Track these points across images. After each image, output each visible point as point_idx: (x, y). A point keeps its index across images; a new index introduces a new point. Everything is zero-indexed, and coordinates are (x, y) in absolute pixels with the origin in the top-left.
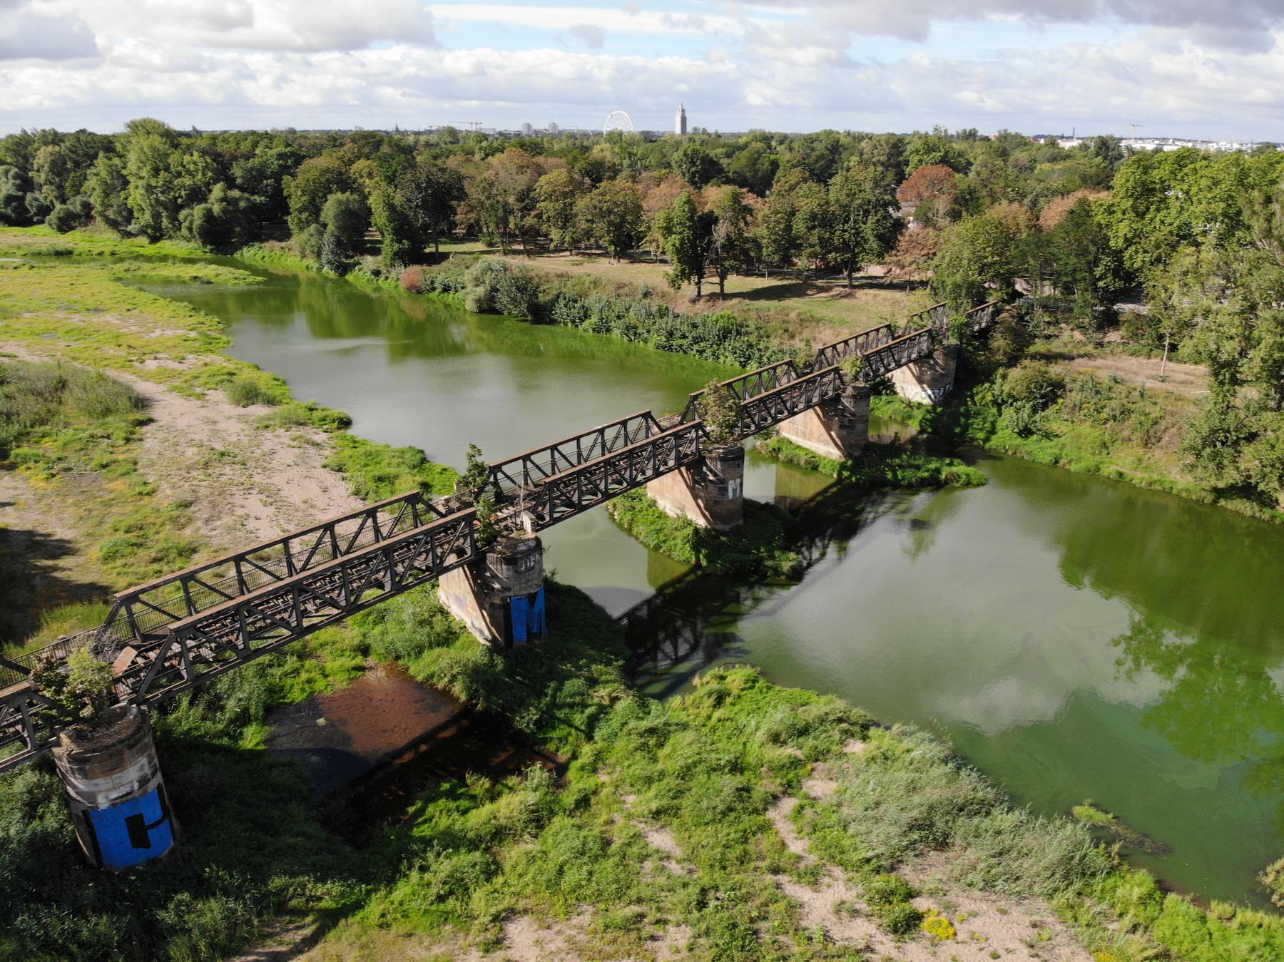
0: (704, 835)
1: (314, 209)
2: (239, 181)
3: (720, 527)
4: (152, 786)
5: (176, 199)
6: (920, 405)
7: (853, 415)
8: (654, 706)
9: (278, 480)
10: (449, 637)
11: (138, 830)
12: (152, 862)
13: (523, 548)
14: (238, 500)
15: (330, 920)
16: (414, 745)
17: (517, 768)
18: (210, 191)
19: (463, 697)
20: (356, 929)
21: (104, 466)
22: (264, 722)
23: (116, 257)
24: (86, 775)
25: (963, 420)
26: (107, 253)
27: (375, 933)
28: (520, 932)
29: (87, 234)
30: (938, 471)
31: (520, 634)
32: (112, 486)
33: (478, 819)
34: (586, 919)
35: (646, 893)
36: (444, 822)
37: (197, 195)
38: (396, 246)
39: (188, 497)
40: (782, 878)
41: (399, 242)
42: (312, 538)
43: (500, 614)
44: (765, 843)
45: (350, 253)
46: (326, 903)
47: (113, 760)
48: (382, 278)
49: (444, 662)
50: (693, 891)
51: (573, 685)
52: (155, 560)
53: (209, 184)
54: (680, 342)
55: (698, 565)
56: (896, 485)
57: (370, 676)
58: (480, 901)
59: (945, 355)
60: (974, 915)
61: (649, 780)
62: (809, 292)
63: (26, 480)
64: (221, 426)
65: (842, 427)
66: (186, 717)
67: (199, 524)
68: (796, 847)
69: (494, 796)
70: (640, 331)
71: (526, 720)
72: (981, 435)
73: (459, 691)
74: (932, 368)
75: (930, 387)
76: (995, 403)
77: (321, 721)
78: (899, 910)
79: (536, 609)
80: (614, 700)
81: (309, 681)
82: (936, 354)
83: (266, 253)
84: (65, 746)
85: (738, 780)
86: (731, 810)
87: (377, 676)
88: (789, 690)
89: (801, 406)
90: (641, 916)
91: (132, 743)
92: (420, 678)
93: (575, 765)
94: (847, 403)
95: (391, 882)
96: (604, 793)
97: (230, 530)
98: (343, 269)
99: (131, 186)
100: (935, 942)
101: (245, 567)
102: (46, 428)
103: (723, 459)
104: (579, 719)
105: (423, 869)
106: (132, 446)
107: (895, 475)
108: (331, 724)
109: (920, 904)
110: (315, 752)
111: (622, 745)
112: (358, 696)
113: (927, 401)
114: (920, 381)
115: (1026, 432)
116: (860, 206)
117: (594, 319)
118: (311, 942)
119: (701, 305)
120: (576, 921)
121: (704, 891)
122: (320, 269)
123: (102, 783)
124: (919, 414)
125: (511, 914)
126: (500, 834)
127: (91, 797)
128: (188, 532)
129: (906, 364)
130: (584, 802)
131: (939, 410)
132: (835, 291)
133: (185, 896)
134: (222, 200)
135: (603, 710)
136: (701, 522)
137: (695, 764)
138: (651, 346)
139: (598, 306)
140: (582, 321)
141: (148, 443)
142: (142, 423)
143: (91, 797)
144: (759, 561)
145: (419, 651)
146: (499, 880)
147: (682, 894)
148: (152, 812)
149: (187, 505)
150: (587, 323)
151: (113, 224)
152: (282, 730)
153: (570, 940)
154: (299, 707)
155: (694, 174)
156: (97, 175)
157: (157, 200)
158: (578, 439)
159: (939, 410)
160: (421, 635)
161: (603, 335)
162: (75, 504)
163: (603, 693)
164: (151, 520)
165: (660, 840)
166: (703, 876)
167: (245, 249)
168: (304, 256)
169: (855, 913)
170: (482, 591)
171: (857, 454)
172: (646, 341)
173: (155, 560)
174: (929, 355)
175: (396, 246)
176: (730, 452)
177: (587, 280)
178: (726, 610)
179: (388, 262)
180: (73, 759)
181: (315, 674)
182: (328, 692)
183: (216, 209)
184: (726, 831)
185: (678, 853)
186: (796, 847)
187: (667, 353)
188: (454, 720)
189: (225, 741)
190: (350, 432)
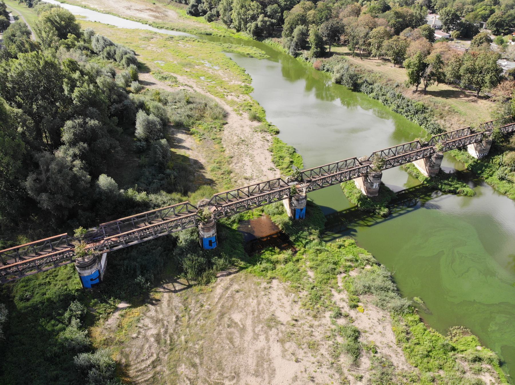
0: (319, 276)
1: (291, 30)
2: (268, 13)
3: (369, 195)
4: (214, 235)
5: (247, 18)
6: (473, 158)
7: (434, 163)
8: (324, 243)
9: (255, 153)
10: (281, 213)
11: (210, 243)
12: (212, 249)
13: (301, 198)
14: (244, 158)
15: (242, 269)
16: (267, 237)
17: (286, 249)
18: (258, 17)
19: (281, 229)
20: (245, 272)
21: (214, 139)
22: (238, 223)
23: (225, 39)
24: (203, 231)
25: (484, 168)
26: (222, 36)
27: (248, 274)
28: (275, 282)
29: (217, 24)
30: (457, 188)
31: (297, 217)
32: (215, 146)
33: (274, 257)
34: (289, 284)
35: (302, 282)
36: (267, 256)
37: (254, 18)
38: (315, 50)
39: (232, 155)
40: (333, 290)
41: (317, 48)
42: (255, 186)
43: (293, 211)
44: (333, 281)
45: (300, 49)
46: (241, 266)
47: (209, 229)
48: (308, 61)
49: (279, 219)
50: (312, 286)
51: (306, 233)
52: (222, 174)
53: (258, 14)
54: (401, 110)
55: (357, 206)
56: (440, 190)
57: (262, 217)
58: (269, 274)
59: (486, 143)
60: (371, 310)
61: (313, 260)
62: (461, 96)
63: (194, 140)
64: (245, 129)
65: (430, 166)
66: (223, 220)
67: (234, 164)
68: (339, 284)
69: (279, 253)
70: (389, 102)
71: (292, 239)
72: (486, 176)
73: (280, 227)
74: (480, 146)
75: (479, 152)
76: (499, 164)
77: (249, 226)
78: (354, 303)
79: (302, 212)
80: (314, 239)
81: (249, 216)
82: (483, 142)
83: (273, 43)
84: (201, 226)
85: (334, 266)
86: (328, 272)
87: (264, 218)
88: (361, 249)
89: (414, 159)
90: (299, 287)
91: (212, 227)
92: (273, 221)
93: (299, 252)
94: (433, 159)
95: (254, 264)
96: (303, 260)
97: (240, 168)
98: (296, 55)
99: (233, 11)
100: (358, 312)
101: (239, 191)
102: (200, 122)
103: (374, 177)
104: (304, 242)
105: (260, 264)
106: (222, 132)
107: (442, 187)
108: (251, 227)
109: (359, 304)
110: (247, 233)
111: (311, 251)
112: (259, 222)
113: (476, 157)
114: (476, 149)
115: (502, 179)
116: (486, 69)
117: (374, 94)
118: (237, 272)
119: (416, 95)
120: (286, 283)
121: (314, 286)
122: (289, 53)
123: (206, 233)
124: (471, 162)
125: (274, 278)
126: (277, 262)
127: (203, 235)
128: (231, 166)
129: (473, 143)
130: (298, 261)
131: (479, 161)
132: (471, 98)
133: (217, 257)
134: (262, 21)
135: (311, 241)
136: (364, 193)
137: (325, 260)
138: (391, 108)
139: (377, 89)
140: (370, 93)
141: (226, 132)
142: (224, 124)
143: (203, 235)
144: (375, 210)
145: (274, 214)
146: (274, 271)
147: (309, 285)
148: (214, 240)
149: (232, 157)
150: (371, 95)
151: (225, 22)
152: (241, 226)
153: (284, 287)
154: (246, 222)
155: (447, 20)
156: (223, 4)
157: (241, 18)
158: (329, 165)
159: (479, 161)
160: (276, 211)
161: (376, 100)
162: (206, 151)
163: (312, 237)
164: (223, 161)
165: (311, 273)
166: (315, 284)
167: (266, 40)
168: (284, 47)
169: (344, 301)
170: (291, 204)
171: (433, 176)
172: (390, 106)
173: (222, 174)
174: (481, 141)
175: (315, 50)
176: (377, 175)
177: (378, 75)
178: (358, 222)
179: (311, 55)
180: (202, 228)
181: (251, 214)
182: (252, 219)
183: (259, 24)
184: (325, 276)
185: (313, 277)
186: (339, 284)
187: (396, 113)
188: (277, 233)
189: (230, 226)
190: (278, 136)
